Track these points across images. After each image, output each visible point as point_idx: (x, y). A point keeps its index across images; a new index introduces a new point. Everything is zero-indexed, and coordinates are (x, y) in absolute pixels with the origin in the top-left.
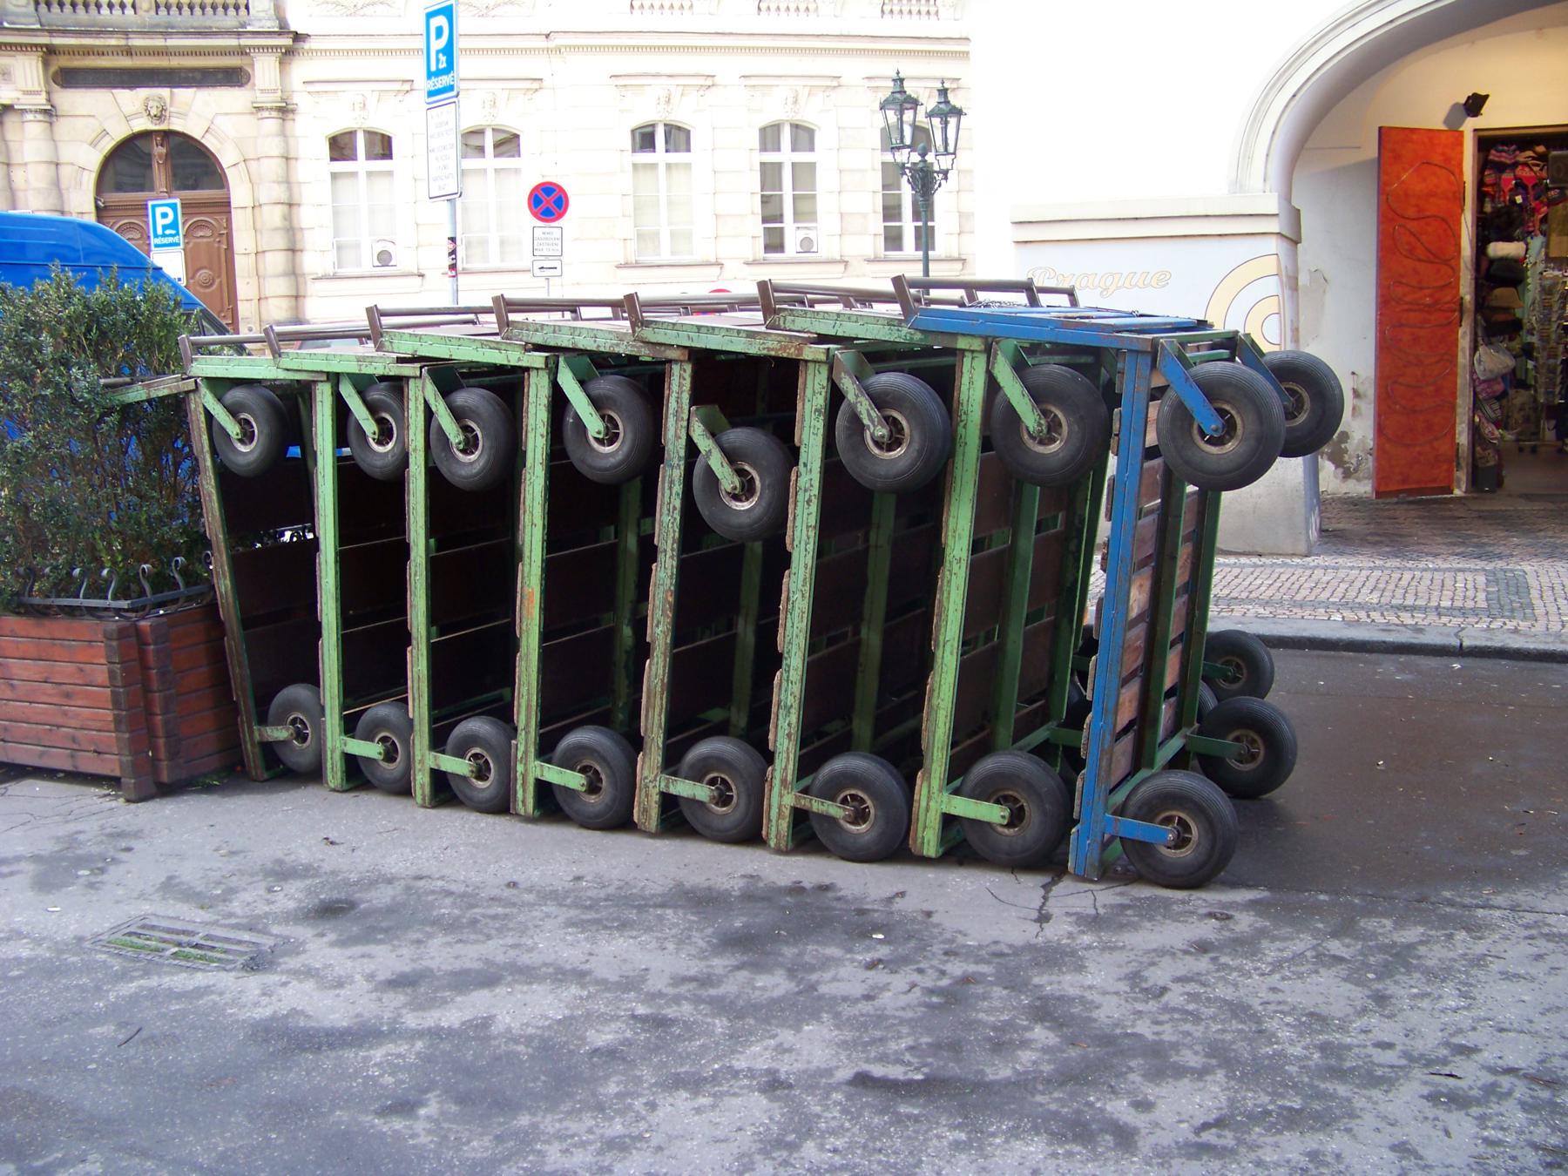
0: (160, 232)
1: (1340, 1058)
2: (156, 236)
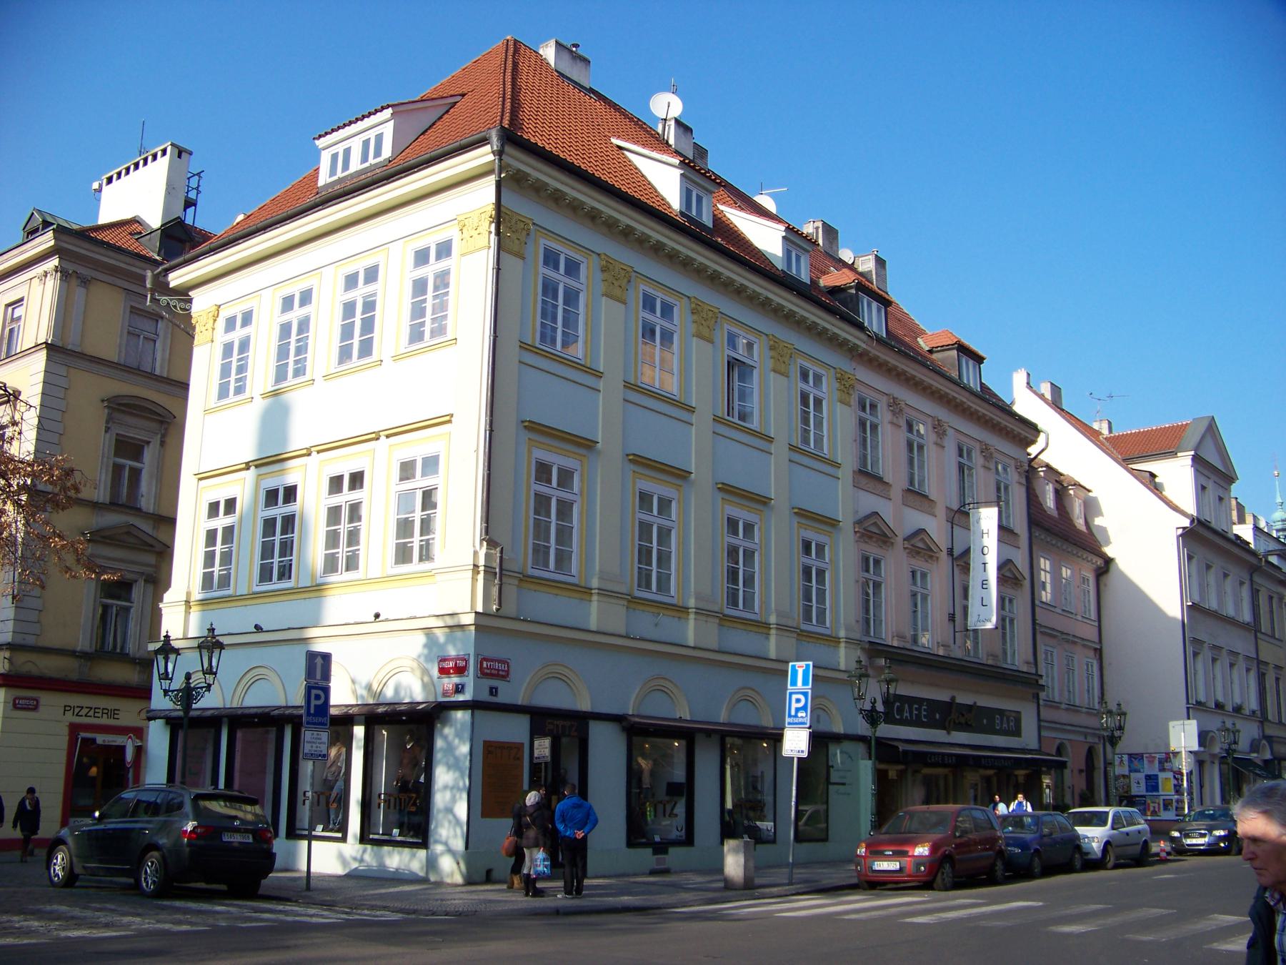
0: (793, 713)
1: (8, 442)
2: (790, 716)
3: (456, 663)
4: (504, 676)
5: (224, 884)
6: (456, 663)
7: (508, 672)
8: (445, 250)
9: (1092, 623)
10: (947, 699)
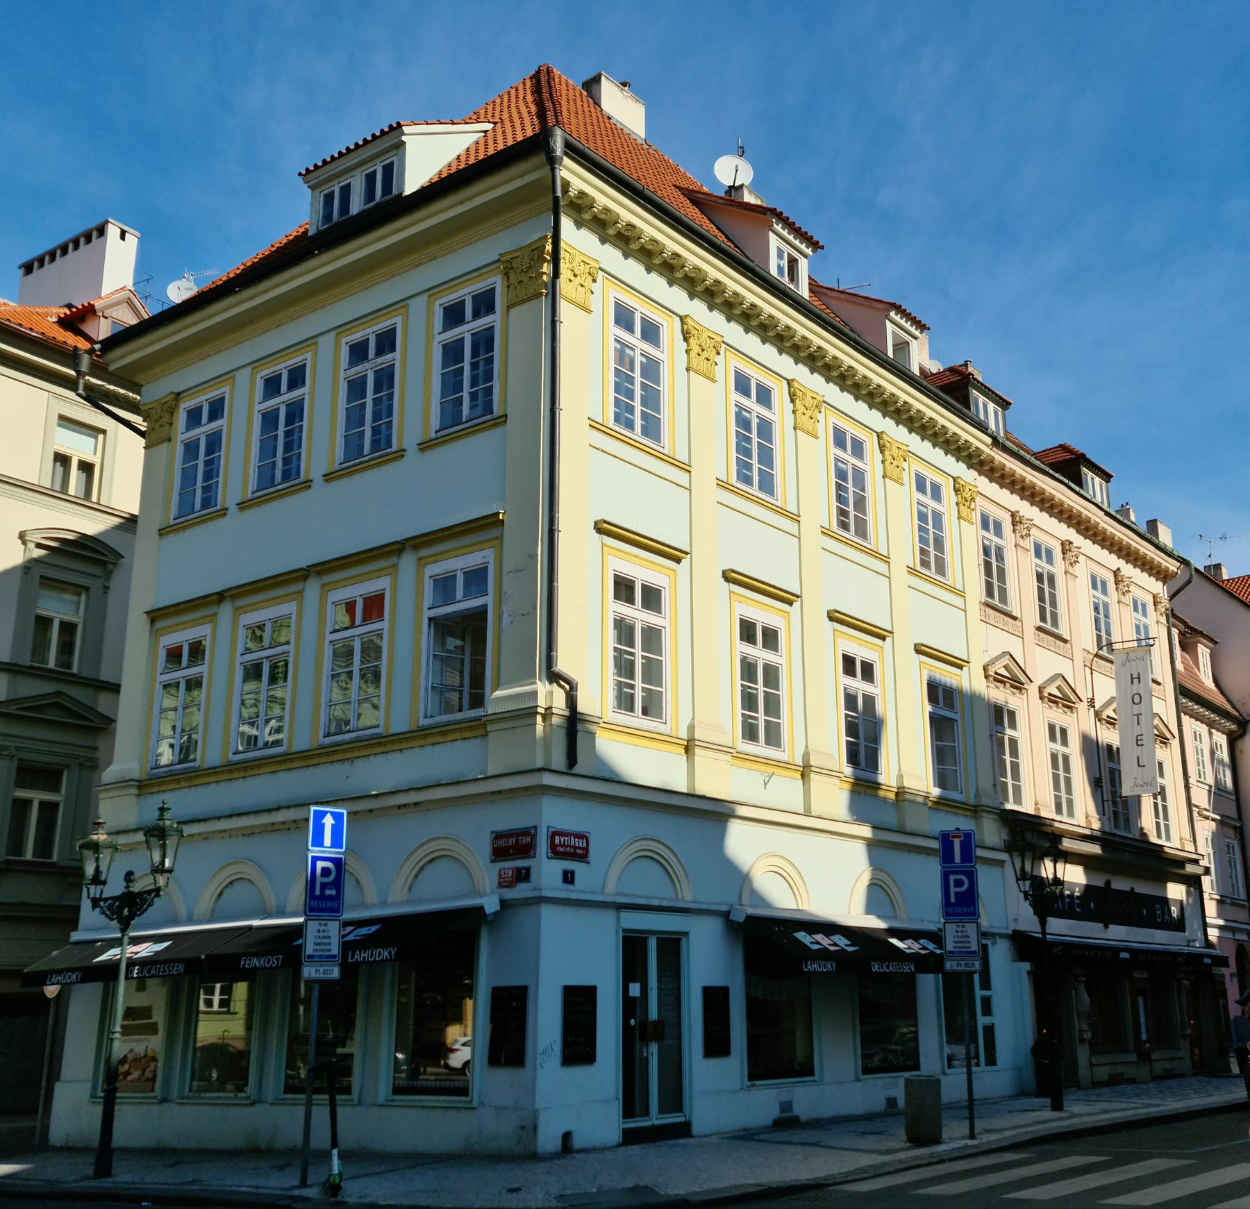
3: (517, 841)
4: (581, 855)
5: (305, 994)
6: (517, 841)
7: (586, 850)
8: (485, 303)
9: (1229, 796)
10: (1128, 889)
